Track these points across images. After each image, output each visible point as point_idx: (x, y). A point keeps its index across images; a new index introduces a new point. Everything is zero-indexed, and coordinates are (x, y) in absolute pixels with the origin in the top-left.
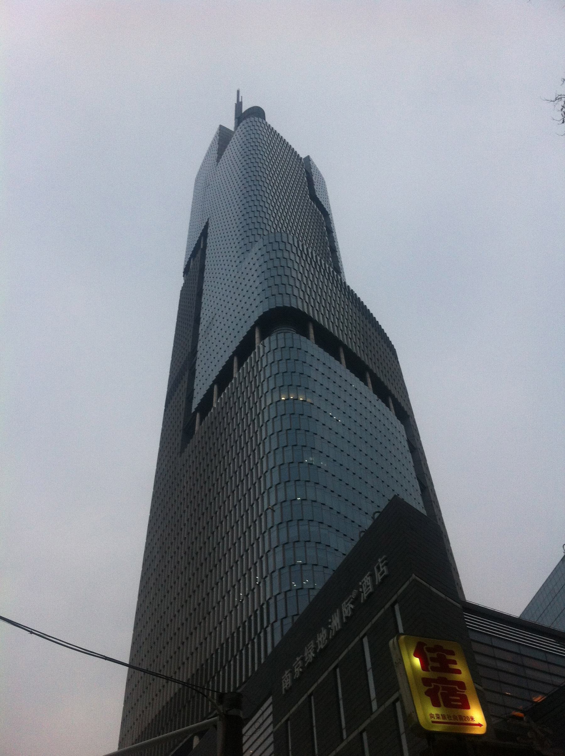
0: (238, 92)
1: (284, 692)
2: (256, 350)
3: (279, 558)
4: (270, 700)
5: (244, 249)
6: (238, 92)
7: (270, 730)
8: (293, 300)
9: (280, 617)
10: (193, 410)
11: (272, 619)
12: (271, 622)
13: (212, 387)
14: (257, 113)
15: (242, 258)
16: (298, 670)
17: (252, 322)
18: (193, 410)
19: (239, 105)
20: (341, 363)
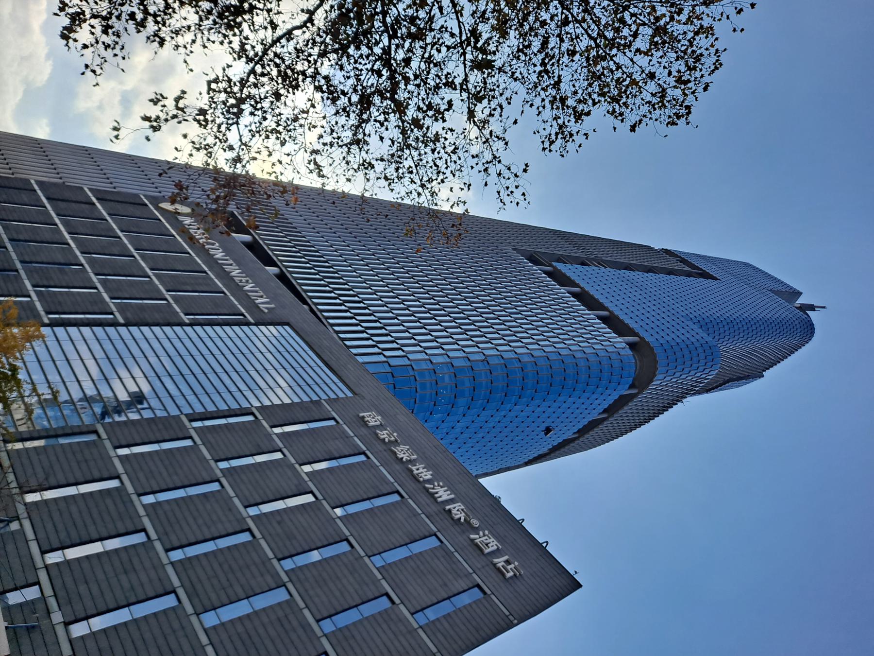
0: (824, 307)
1: (361, 415)
2: (587, 312)
3: (440, 359)
4: (350, 394)
5: (703, 323)
6: (824, 307)
7: (324, 397)
8: (662, 376)
9: (390, 360)
10: (554, 264)
11: (387, 353)
12: (384, 353)
13: (577, 286)
14: (808, 331)
15: (695, 320)
16: (384, 434)
17: (642, 334)
18: (554, 264)
19: (812, 308)
20: (600, 414)
